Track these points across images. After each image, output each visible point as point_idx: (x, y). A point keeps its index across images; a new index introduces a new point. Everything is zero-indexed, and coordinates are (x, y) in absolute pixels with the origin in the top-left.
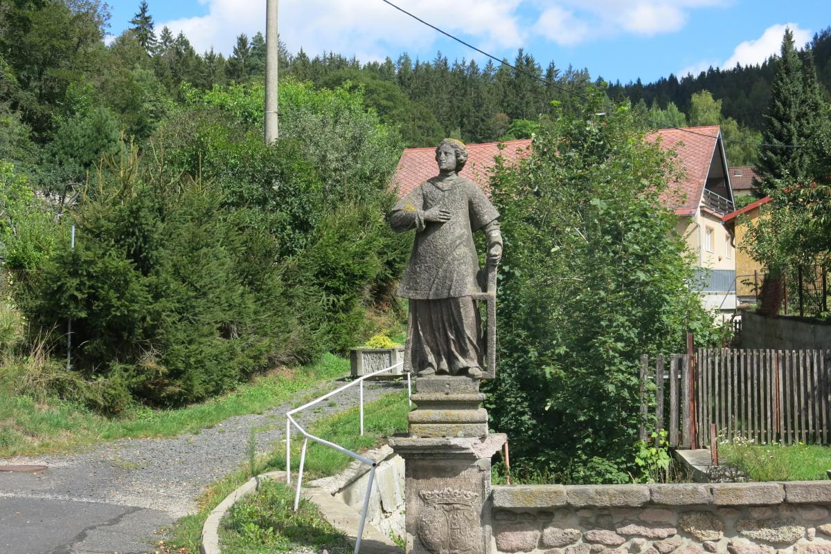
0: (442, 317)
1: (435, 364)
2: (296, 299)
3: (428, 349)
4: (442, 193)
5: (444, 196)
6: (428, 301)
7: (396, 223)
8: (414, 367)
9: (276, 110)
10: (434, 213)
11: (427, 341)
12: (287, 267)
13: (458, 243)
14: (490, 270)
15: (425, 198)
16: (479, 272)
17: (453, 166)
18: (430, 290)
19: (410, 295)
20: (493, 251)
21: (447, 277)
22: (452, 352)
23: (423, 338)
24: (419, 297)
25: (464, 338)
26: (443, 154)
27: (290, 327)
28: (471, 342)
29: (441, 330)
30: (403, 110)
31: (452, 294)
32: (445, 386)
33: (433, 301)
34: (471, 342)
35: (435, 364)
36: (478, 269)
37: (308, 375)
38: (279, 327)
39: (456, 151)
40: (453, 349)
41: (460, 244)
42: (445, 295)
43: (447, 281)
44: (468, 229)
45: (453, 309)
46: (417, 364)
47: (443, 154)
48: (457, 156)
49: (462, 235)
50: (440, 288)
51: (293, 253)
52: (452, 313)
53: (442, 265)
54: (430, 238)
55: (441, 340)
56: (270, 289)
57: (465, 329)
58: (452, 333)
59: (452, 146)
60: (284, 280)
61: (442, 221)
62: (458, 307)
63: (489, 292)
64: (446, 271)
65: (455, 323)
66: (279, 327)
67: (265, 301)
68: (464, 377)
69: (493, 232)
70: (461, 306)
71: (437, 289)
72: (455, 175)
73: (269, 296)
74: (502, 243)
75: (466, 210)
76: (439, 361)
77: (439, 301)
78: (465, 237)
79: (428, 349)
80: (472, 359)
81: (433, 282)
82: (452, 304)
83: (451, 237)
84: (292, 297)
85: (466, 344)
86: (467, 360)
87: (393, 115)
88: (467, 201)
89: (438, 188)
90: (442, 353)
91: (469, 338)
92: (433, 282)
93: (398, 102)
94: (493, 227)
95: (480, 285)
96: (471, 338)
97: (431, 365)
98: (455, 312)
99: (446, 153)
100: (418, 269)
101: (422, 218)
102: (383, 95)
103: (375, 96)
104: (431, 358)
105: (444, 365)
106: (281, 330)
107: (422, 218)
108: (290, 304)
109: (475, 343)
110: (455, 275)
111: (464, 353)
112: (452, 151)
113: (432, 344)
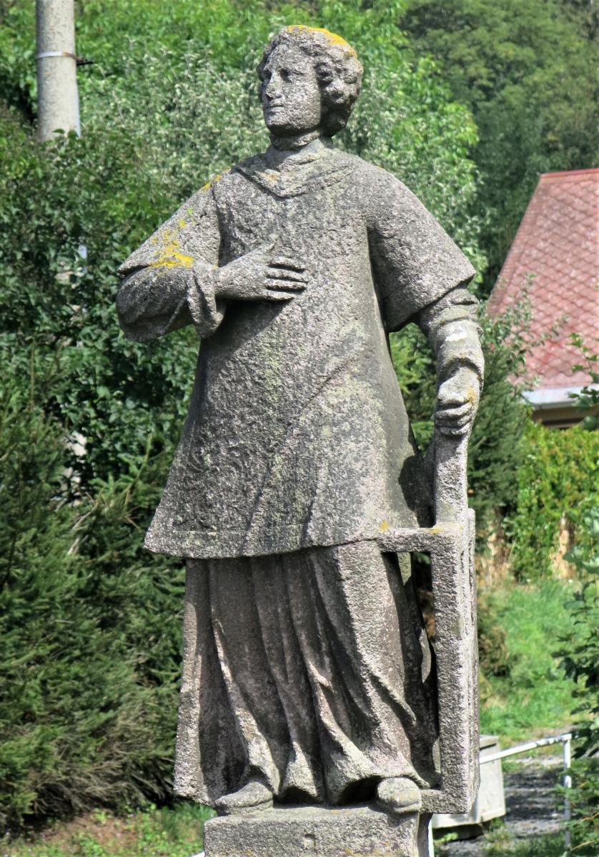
0: (289, 613)
1: (270, 770)
2: (130, 607)
3: (247, 723)
4: (276, 206)
5: (283, 215)
6: (244, 560)
7: (132, 309)
8: (210, 783)
9: (71, 50)
10: (249, 272)
11: (246, 696)
12: (98, 513)
13: (330, 367)
14: (442, 452)
15: (224, 223)
16: (409, 463)
17: (311, 115)
18: (248, 526)
19: (186, 544)
20: (447, 391)
21: (299, 481)
22: (326, 730)
23: (231, 687)
24: (212, 551)
25: (359, 681)
26: (276, 78)
27: (111, 693)
28: (385, 694)
29: (288, 659)
30: (562, 69)
31: (313, 534)
32: (297, 843)
33: (259, 559)
34: (385, 694)
35: (270, 770)
36: (407, 450)
37: (174, 837)
38: (76, 694)
39: (317, 67)
40: (327, 718)
41: (338, 370)
42: (292, 543)
43: (298, 493)
44: (368, 324)
45: (321, 584)
46: (218, 774)
47: (276, 78)
48: (323, 80)
49: (347, 341)
50: (277, 517)
51: (120, 469)
52: (319, 598)
53: (280, 443)
54: (241, 353)
55: (289, 690)
56: (32, 578)
57: (362, 650)
58: (321, 666)
59: (305, 51)
60: (88, 551)
61: (277, 295)
62: (335, 579)
63: (439, 528)
64: (293, 461)
65: (330, 631)
66: (76, 694)
67: (18, 614)
68: (364, 812)
69: (450, 328)
70: (345, 573)
71: (270, 523)
72: (318, 144)
73: (30, 598)
74: (480, 361)
75: (360, 257)
76: (284, 759)
77: (279, 558)
78: (358, 347)
79: (247, 723)
80: (390, 751)
81: (257, 501)
82: (318, 570)
83: (308, 348)
84: (116, 601)
85: (367, 701)
86: (375, 753)
87: (536, 85)
88: (362, 229)
89: (264, 189)
90: (293, 734)
91: (375, 680)
92: (257, 501)
93: (547, 48)
94: (450, 312)
95: (411, 503)
96: (385, 681)
97: (258, 774)
98: (327, 596)
99: (285, 74)
100: (208, 460)
101: (210, 290)
102: (504, 28)
103: (481, 33)
104: (260, 752)
105: (302, 774)
106: (82, 700)
107: (210, 290)
108: (105, 624)
109: (399, 695)
110: (323, 473)
111: (363, 730)
112: (306, 65)
113: (264, 706)
